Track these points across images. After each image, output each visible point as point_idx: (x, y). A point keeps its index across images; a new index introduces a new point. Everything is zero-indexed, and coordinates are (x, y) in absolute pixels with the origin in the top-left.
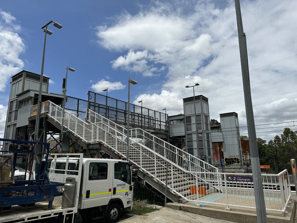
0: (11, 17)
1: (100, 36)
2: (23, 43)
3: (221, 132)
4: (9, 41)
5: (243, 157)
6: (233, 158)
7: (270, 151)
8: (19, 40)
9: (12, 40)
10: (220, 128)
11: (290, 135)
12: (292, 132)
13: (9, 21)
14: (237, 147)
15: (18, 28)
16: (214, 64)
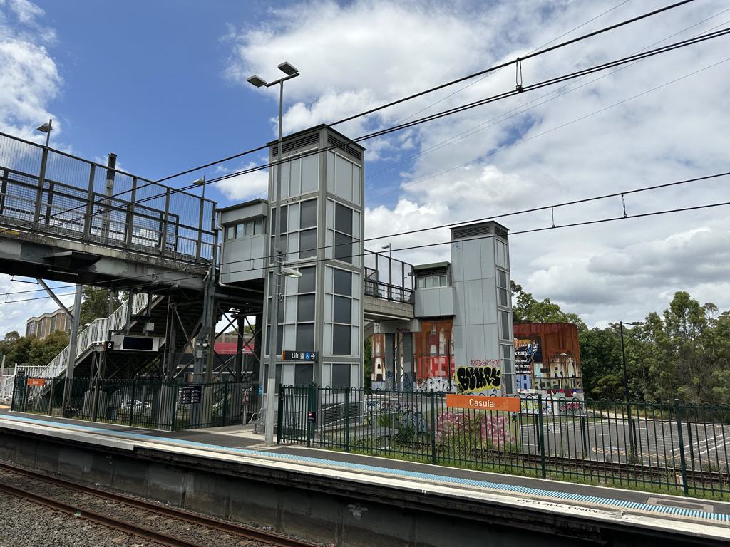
0: (33, 6)
1: (242, 54)
2: (59, 75)
3: (451, 285)
4: (23, 68)
5: (556, 369)
6: (481, 369)
7: (632, 354)
8: (49, 66)
9: (30, 64)
10: (448, 272)
11: (687, 311)
12: (696, 305)
13: (27, 18)
14: (494, 333)
15: (49, 35)
16: (534, 140)
